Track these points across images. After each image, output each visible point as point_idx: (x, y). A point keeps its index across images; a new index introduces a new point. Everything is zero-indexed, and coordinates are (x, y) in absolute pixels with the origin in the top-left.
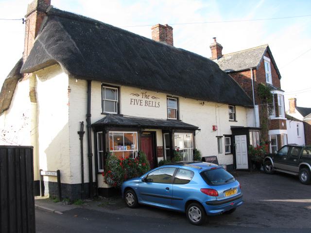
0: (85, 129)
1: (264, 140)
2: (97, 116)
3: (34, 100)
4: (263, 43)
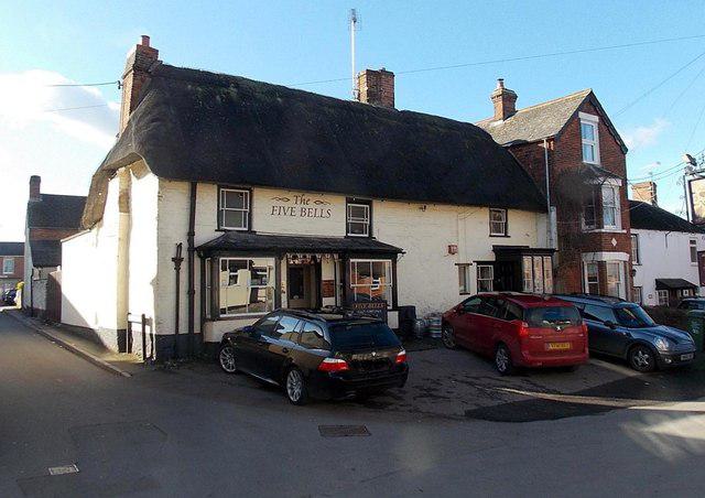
0: (184, 254)
1: (347, 300)
2: (207, 231)
3: (125, 209)
4: (578, 91)
